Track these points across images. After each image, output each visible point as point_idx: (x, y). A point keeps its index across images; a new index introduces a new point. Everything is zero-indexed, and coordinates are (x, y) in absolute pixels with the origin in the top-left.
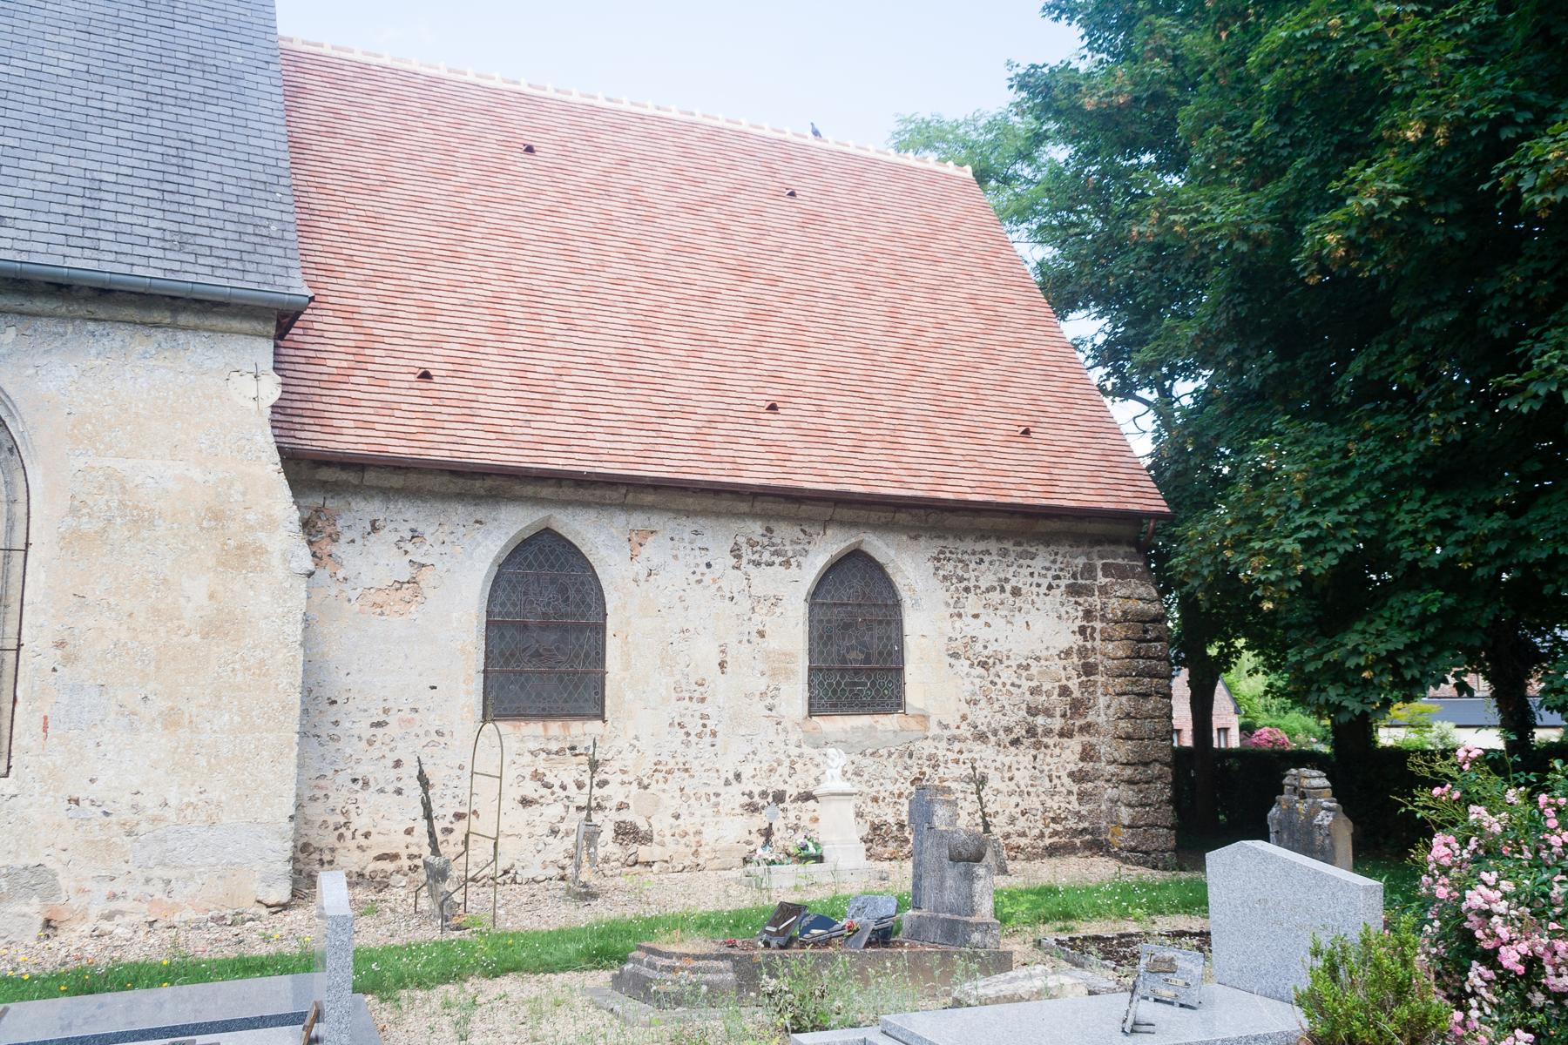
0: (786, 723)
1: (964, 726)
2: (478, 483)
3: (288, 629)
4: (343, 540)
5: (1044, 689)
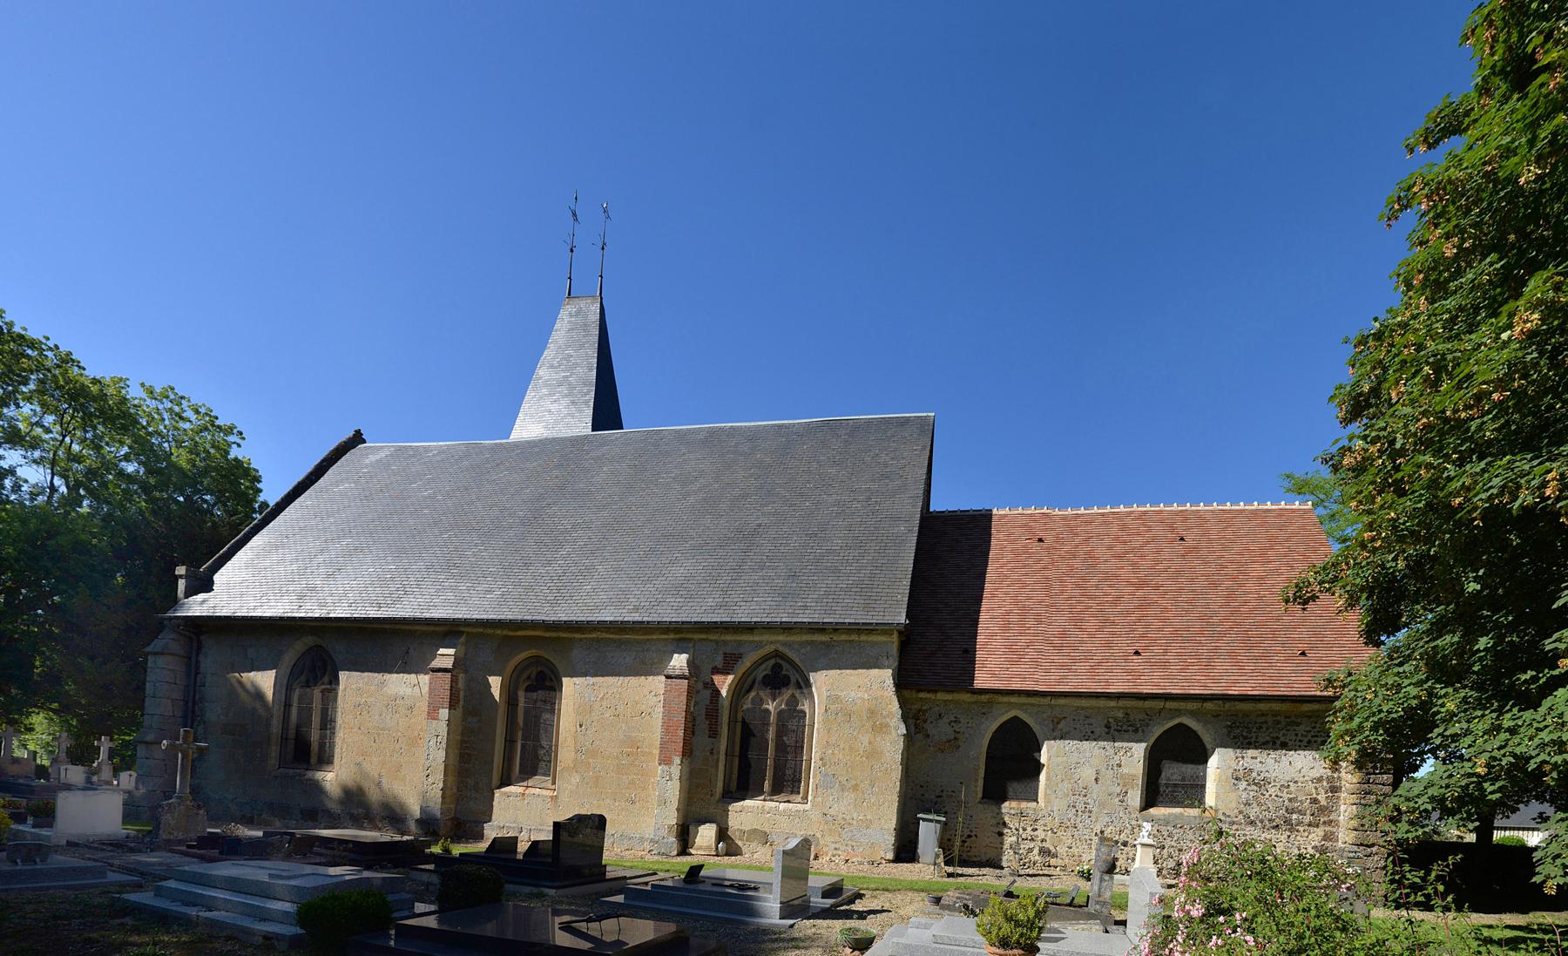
0: (1130, 809)
1: (1241, 816)
2: (983, 697)
3: (896, 756)
4: (928, 722)
5: (1299, 799)
